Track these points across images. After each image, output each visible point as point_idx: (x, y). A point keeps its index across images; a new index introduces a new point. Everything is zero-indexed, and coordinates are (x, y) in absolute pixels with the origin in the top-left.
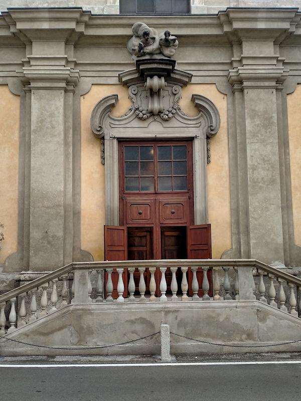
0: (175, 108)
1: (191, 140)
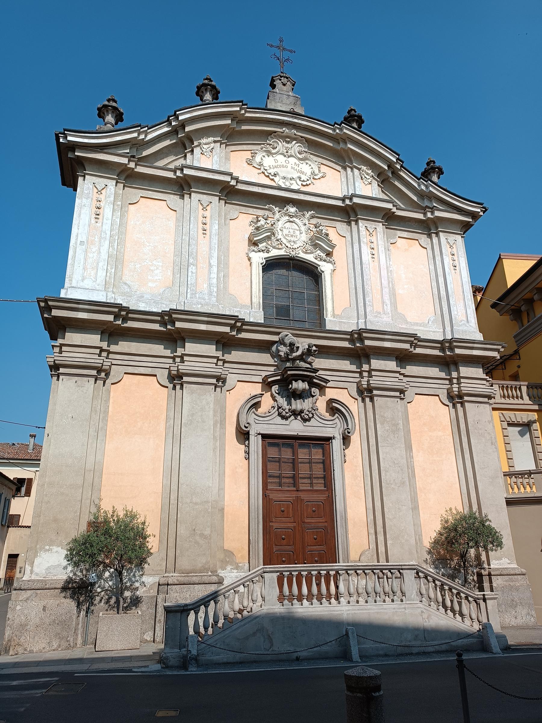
0: (315, 409)
1: (329, 439)
